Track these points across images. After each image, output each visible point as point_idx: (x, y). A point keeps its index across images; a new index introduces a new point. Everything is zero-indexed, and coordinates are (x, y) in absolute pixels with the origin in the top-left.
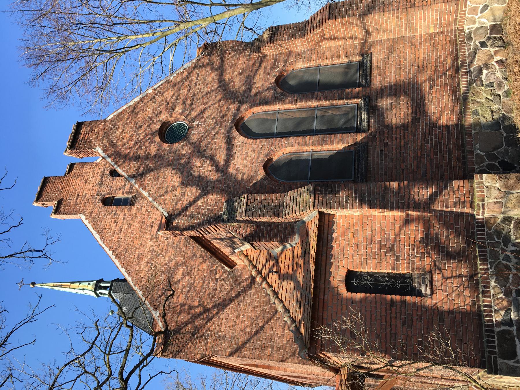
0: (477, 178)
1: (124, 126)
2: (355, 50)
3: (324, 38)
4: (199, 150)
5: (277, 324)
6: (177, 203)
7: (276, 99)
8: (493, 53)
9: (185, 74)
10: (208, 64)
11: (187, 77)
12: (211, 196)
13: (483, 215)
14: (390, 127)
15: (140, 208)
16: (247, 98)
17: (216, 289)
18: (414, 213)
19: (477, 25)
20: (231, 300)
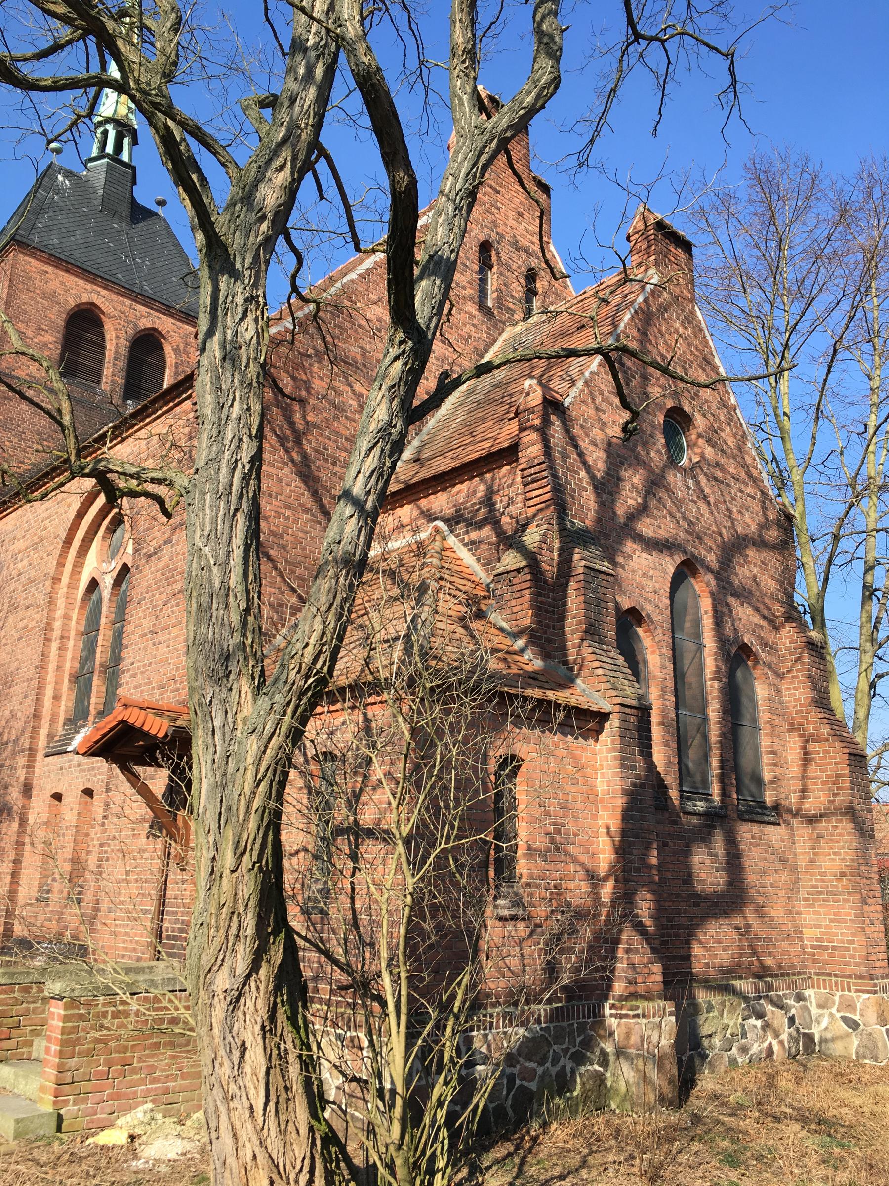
0: (670, 1007)
1: (687, 339)
2: (783, 796)
3: (807, 741)
4: (656, 484)
5: (273, 590)
6: (582, 427)
7: (723, 642)
8: (781, 1037)
9: (755, 473)
10: (767, 519)
11: (750, 476)
12: (592, 497)
13: (612, 1015)
14: (688, 853)
15: (475, 321)
16: (724, 588)
17: (334, 463)
18: (607, 891)
19: (814, 1011)
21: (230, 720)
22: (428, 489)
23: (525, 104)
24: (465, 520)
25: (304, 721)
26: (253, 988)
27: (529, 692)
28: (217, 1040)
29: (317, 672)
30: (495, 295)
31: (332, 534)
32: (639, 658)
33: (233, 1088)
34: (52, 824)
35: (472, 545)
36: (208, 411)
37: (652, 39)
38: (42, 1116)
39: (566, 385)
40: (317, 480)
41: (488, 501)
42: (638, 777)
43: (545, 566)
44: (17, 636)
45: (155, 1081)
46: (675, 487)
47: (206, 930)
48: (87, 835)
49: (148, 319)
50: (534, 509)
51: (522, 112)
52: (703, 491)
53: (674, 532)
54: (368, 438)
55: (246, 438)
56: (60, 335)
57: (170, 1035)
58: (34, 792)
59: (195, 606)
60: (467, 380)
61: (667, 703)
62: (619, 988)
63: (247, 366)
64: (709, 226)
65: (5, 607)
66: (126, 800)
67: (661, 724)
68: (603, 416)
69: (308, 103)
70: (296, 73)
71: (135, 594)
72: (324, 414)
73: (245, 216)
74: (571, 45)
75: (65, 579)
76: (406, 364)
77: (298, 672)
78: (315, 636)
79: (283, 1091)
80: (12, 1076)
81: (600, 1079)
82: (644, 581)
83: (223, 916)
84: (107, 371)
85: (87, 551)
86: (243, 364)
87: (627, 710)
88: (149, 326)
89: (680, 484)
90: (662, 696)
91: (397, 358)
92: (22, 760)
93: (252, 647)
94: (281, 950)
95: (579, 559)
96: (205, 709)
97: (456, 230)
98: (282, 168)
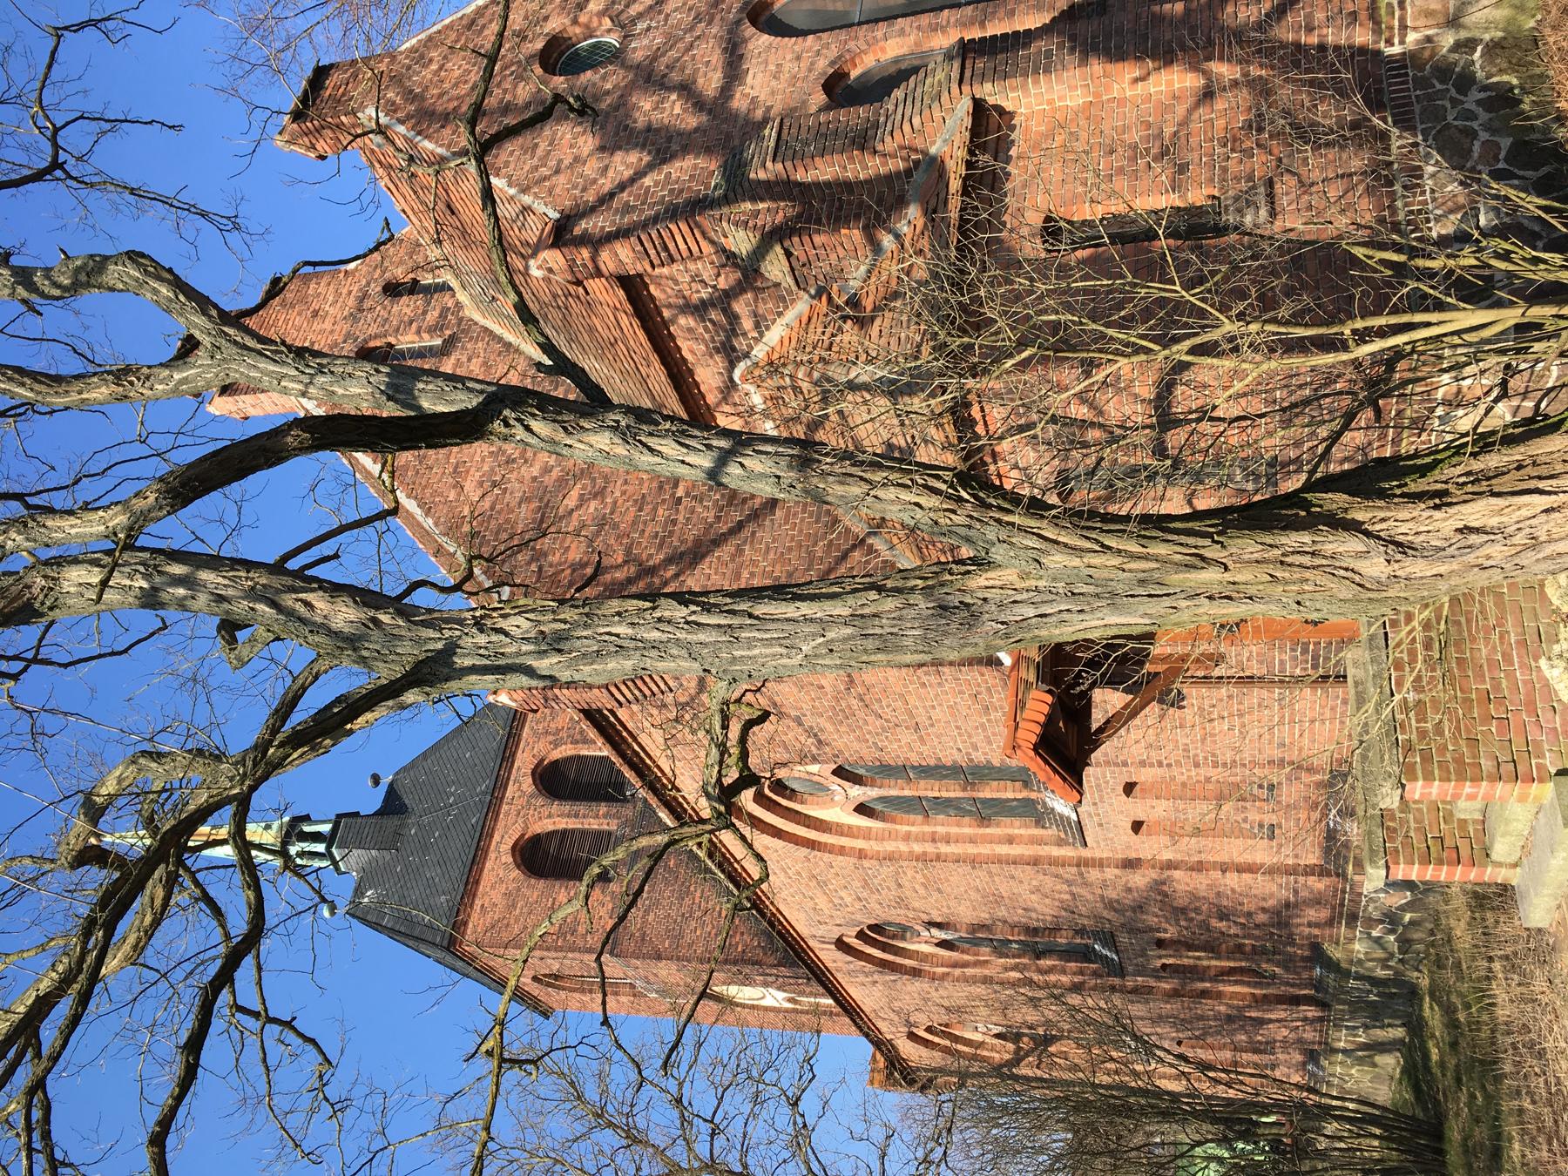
1: (445, 58)
6: (584, 190)
12: (678, 164)
13: (1402, 42)
15: (464, 359)
17: (674, 522)
18: (1224, 70)
20: (718, 542)
21: (1025, 596)
22: (692, 395)
23: (171, 295)
24: (728, 339)
25: (1015, 499)
26: (1384, 526)
27: (954, 215)
28: (1455, 567)
29: (951, 486)
30: (425, 336)
31: (768, 489)
32: (892, 70)
33: (1519, 539)
34: (1174, 832)
35: (760, 325)
36: (629, 664)
37: (56, 147)
38: (1559, 795)
39: (531, 219)
40: (698, 542)
41: (699, 309)
42: (1061, 46)
43: (779, 218)
44: (936, 895)
45: (1507, 658)
46: (649, 48)
47: (1306, 596)
48: (1184, 785)
49: (521, 782)
50: (703, 243)
51: (182, 298)
52: (651, 7)
53: (712, 41)
54: (637, 455)
55: (657, 614)
56: (558, 884)
57: (1451, 636)
58: (1134, 855)
59: (881, 657)
60: (542, 334)
61: (952, 20)
62: (1362, 36)
63: (565, 622)
64: (288, 47)
65: (902, 912)
66: (1138, 745)
67: (982, 25)
68: (566, 162)
69: (220, 580)
70: (185, 598)
71: (869, 755)
72: (612, 541)
73: (375, 642)
74: (82, 248)
75: (859, 844)
76: (533, 415)
77: (954, 512)
78: (906, 496)
79: (1522, 472)
80: (1508, 839)
81: (1493, 48)
82: (785, 76)
83: (1287, 575)
84: (593, 824)
85: (822, 821)
86: (563, 626)
87: (968, 74)
88: (530, 780)
89: (645, 42)
90: (944, 29)
91: (528, 428)
92: (1094, 875)
93: (926, 579)
94: (1330, 495)
95: (764, 171)
96: (1012, 629)
97: (349, 369)
98: (307, 604)
